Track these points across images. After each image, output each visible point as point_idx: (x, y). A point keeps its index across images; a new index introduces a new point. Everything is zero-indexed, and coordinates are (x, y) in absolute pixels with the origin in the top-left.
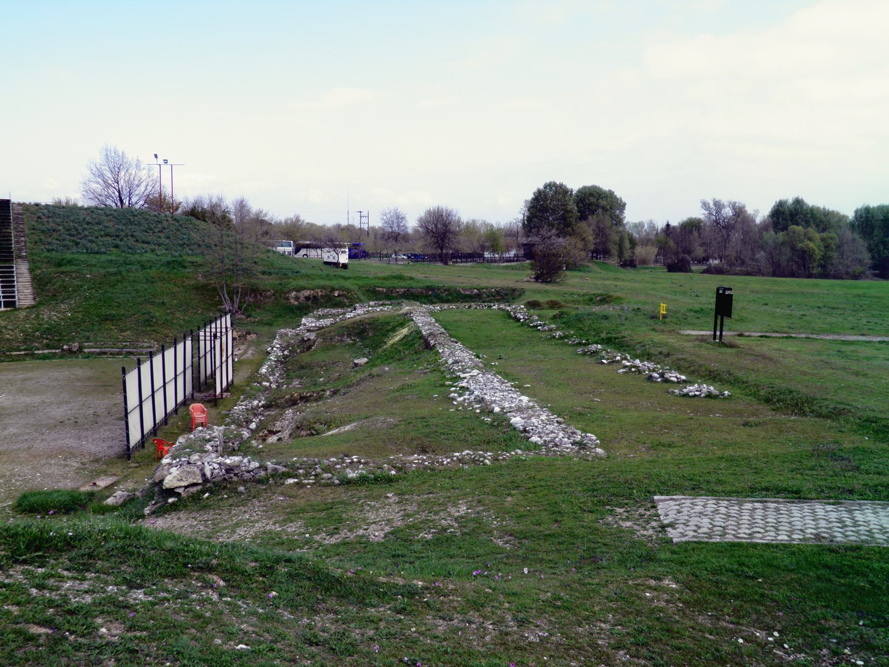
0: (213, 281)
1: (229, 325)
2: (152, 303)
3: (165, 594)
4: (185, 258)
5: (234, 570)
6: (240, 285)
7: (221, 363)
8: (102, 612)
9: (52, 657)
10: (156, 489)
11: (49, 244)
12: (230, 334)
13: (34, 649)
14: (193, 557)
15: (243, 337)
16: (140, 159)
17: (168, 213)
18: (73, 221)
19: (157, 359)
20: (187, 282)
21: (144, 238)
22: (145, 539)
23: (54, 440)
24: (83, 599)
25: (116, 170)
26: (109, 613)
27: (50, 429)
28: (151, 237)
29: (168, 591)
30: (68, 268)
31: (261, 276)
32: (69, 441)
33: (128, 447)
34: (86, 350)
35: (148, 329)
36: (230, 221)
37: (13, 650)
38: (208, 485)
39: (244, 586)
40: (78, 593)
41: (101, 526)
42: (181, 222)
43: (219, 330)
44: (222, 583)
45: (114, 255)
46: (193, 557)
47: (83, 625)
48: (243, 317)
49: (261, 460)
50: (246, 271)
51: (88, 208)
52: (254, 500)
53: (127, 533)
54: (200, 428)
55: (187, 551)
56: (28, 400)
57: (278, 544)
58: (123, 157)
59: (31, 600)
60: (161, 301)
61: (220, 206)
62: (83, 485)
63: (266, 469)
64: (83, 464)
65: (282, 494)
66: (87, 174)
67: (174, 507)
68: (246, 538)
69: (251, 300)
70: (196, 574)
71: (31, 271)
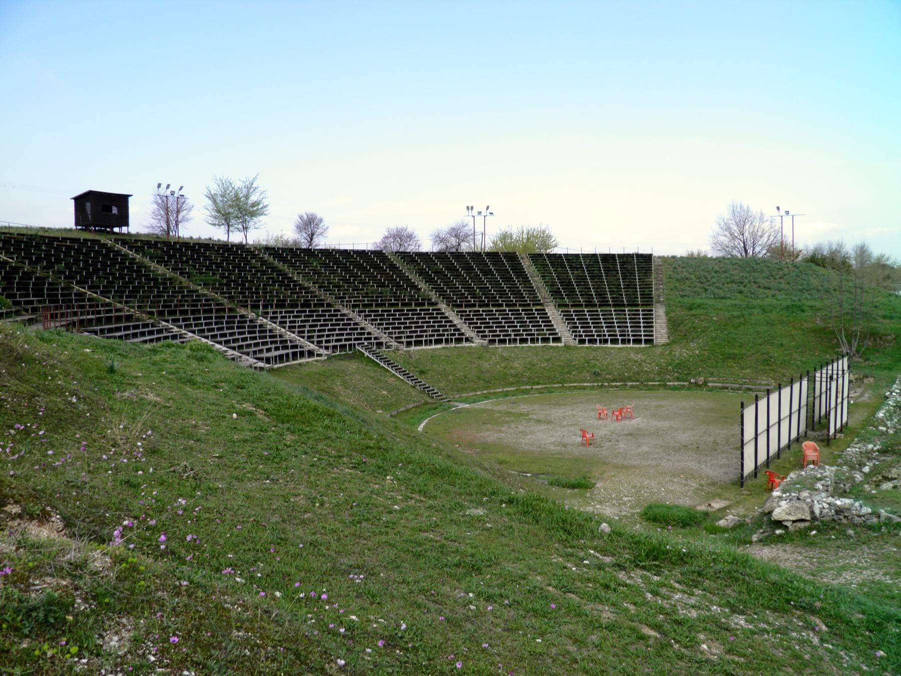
0: (831, 324)
1: (846, 368)
2: (772, 344)
3: (765, 626)
4: (804, 302)
5: (838, 618)
6: (859, 328)
7: (836, 404)
8: (705, 629)
9: (658, 660)
10: (765, 519)
11: (683, 290)
12: (846, 376)
13: (644, 648)
14: (796, 595)
15: (860, 380)
16: (764, 212)
17: (788, 260)
18: (703, 270)
19: (774, 397)
20: (806, 325)
21: (766, 285)
22: (750, 567)
23: (678, 461)
24: (690, 612)
25: (741, 224)
26: (711, 631)
27: (675, 451)
28: (772, 283)
29: (769, 624)
30: (698, 312)
31: (881, 320)
32: (690, 463)
33: (742, 475)
34: (710, 384)
35: (767, 368)
36: (850, 266)
37: (627, 644)
38: (816, 523)
39: (848, 636)
40: (686, 606)
41: (712, 548)
42: (801, 269)
43: (835, 372)
44: (824, 628)
45: (738, 300)
46: (796, 595)
47: (687, 637)
48: (860, 360)
49: (873, 506)
50: (866, 315)
51: (717, 258)
52: (864, 546)
53: (735, 559)
54: (812, 466)
55: (791, 588)
56: (659, 424)
57: (887, 597)
58: (748, 211)
59: (645, 603)
60: (780, 342)
61: (839, 252)
62: (700, 504)
63: (879, 516)
64: (700, 485)
65: (895, 545)
66: (717, 228)
67: (781, 539)
68: (852, 583)
69: (870, 343)
70: (798, 613)
71: (667, 313)
